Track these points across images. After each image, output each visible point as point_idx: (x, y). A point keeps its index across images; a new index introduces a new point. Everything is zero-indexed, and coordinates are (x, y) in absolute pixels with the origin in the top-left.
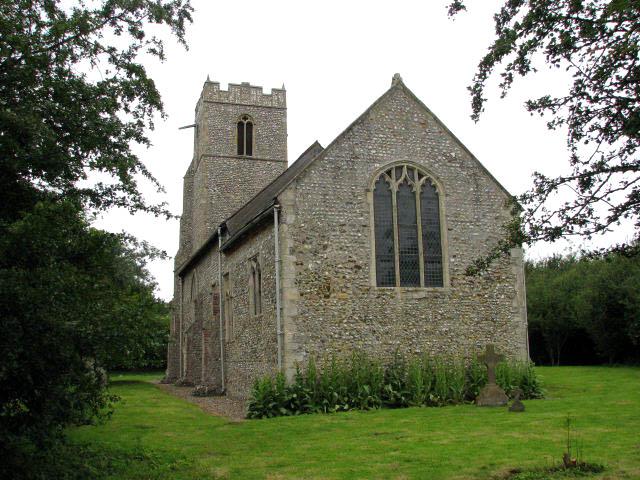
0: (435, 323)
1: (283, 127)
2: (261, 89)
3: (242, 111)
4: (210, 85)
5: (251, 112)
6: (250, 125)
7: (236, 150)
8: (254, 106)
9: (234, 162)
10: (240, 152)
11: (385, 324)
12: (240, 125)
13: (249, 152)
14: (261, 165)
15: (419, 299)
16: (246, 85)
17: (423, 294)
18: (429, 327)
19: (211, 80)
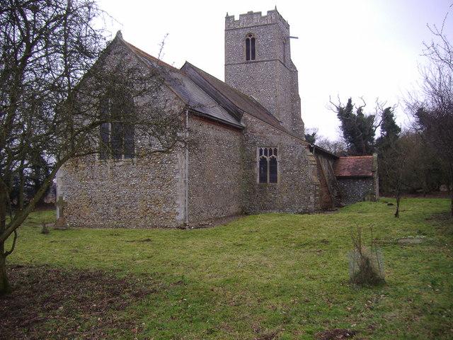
0: (128, 180)
1: (138, 52)
2: (260, 13)
3: (248, 31)
4: (229, 19)
5: (255, 32)
6: (253, 40)
7: (245, 58)
8: (255, 26)
9: (244, 66)
10: (248, 59)
11: (102, 180)
12: (248, 40)
13: (254, 58)
14: (261, 64)
15: (120, 166)
16: (251, 14)
17: (121, 163)
18: (124, 182)
19: (229, 15)
